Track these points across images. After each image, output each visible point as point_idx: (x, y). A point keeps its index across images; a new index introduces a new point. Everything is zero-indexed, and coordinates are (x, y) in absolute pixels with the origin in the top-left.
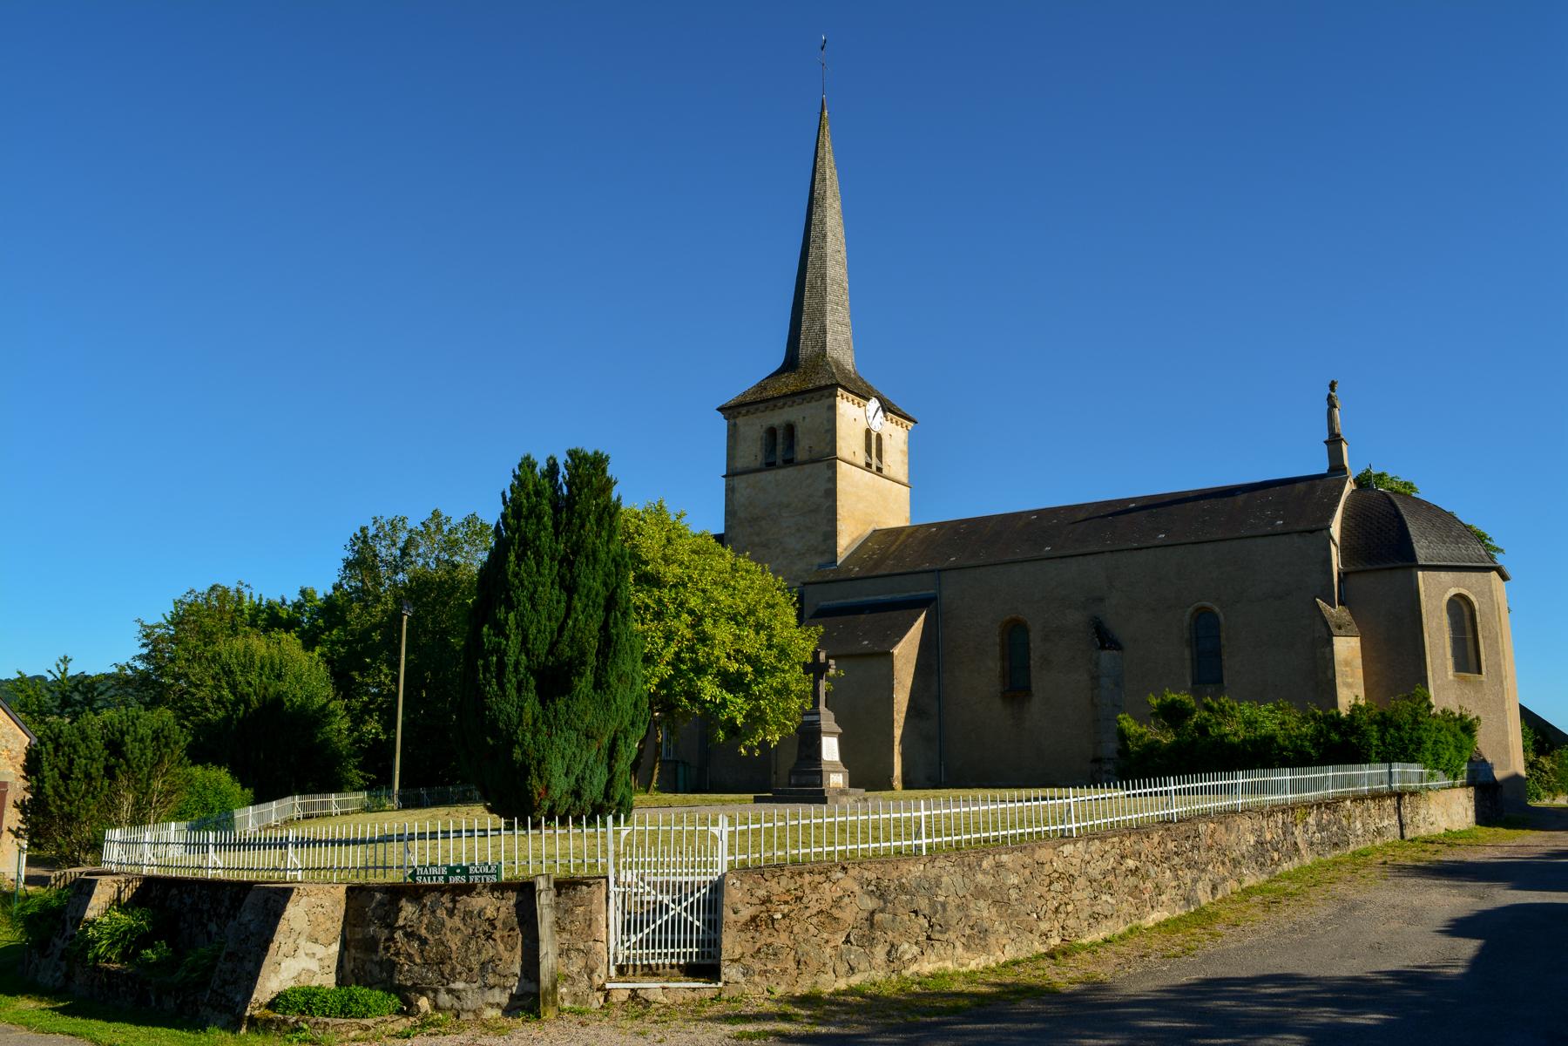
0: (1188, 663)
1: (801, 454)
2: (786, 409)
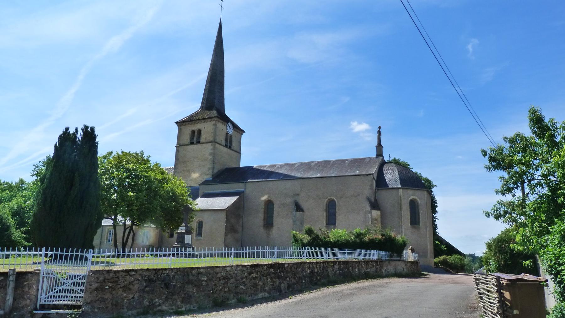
0: (325, 217)
1: (202, 140)
2: (199, 124)
